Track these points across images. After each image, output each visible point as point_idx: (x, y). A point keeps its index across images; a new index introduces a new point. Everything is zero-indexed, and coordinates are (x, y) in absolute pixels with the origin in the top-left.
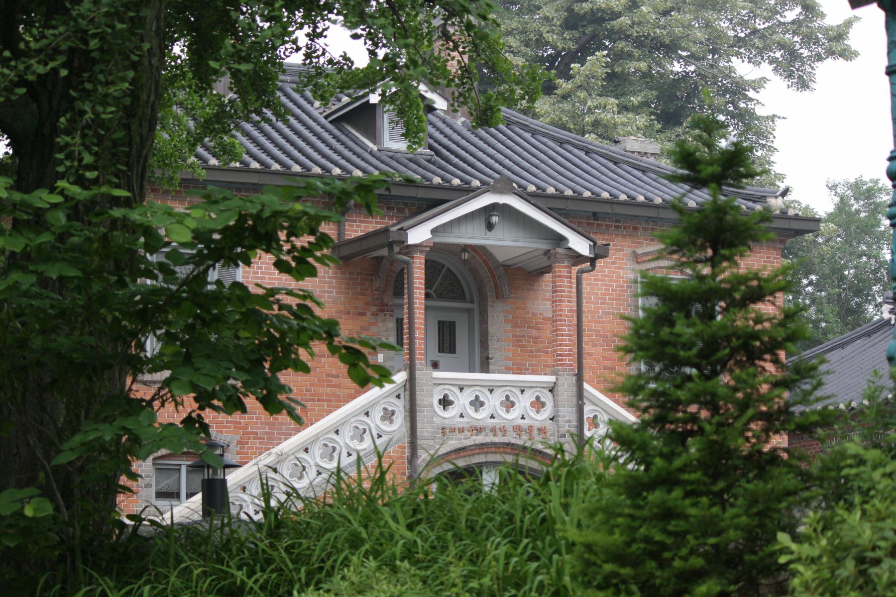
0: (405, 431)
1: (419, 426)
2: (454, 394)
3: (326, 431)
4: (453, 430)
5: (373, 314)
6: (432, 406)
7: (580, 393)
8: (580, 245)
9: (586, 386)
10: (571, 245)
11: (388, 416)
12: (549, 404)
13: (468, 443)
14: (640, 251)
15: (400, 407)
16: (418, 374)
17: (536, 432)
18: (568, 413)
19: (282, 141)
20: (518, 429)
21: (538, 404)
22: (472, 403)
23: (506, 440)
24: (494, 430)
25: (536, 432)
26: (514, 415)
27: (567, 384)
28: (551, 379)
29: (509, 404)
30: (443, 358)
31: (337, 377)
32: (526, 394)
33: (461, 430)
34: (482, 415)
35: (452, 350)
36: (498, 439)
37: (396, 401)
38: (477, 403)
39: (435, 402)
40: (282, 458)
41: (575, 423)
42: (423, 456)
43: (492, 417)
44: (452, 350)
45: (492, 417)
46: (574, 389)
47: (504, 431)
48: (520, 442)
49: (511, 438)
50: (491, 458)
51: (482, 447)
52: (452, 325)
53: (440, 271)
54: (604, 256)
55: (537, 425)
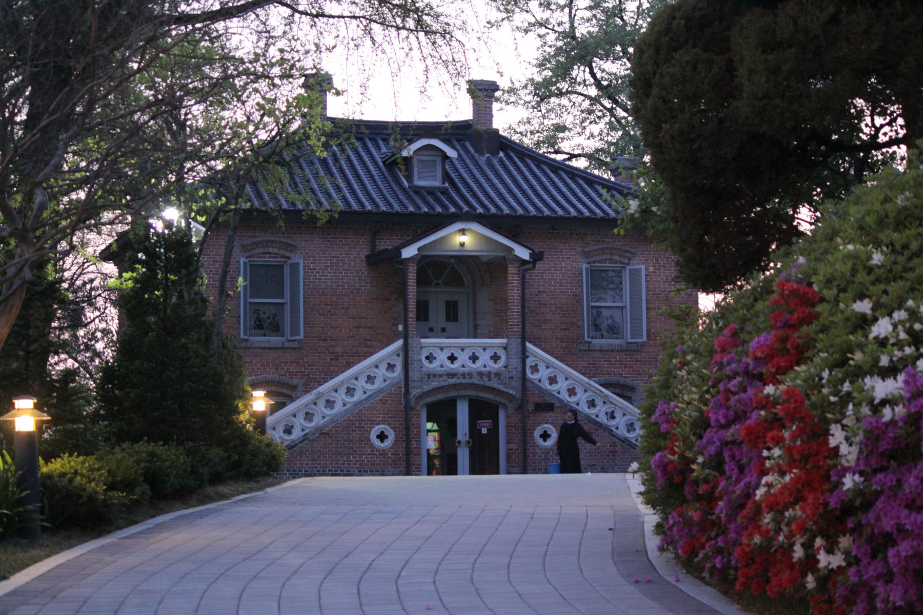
0: (402, 377)
1: (411, 374)
2: (437, 353)
3: (349, 379)
4: (435, 376)
5: (395, 299)
6: (420, 361)
7: (524, 349)
8: (523, 253)
9: (528, 344)
10: (516, 253)
11: (391, 367)
12: (503, 357)
13: (444, 384)
14: (245, 243)
15: (399, 362)
16: (410, 340)
17: (493, 376)
18: (516, 363)
19: (503, 190)
20: (481, 374)
21: (495, 358)
22: (449, 358)
23: (470, 381)
24: (463, 375)
25: (493, 376)
26: (478, 365)
27: (515, 343)
28: (504, 341)
29: (474, 358)
30: (450, 326)
31: (370, 340)
32: (487, 351)
33: (441, 376)
34: (456, 365)
35: (456, 320)
36: (467, 381)
37: (396, 358)
38: (452, 358)
39: (423, 358)
40: (320, 395)
41: (520, 369)
42: (414, 392)
43: (463, 366)
44: (456, 320)
45: (463, 366)
46: (520, 348)
47: (470, 375)
48: (481, 383)
49: (476, 380)
50: (462, 393)
51: (454, 386)
52: (455, 304)
53: (581, 274)
54: (541, 259)
55: (494, 371)
